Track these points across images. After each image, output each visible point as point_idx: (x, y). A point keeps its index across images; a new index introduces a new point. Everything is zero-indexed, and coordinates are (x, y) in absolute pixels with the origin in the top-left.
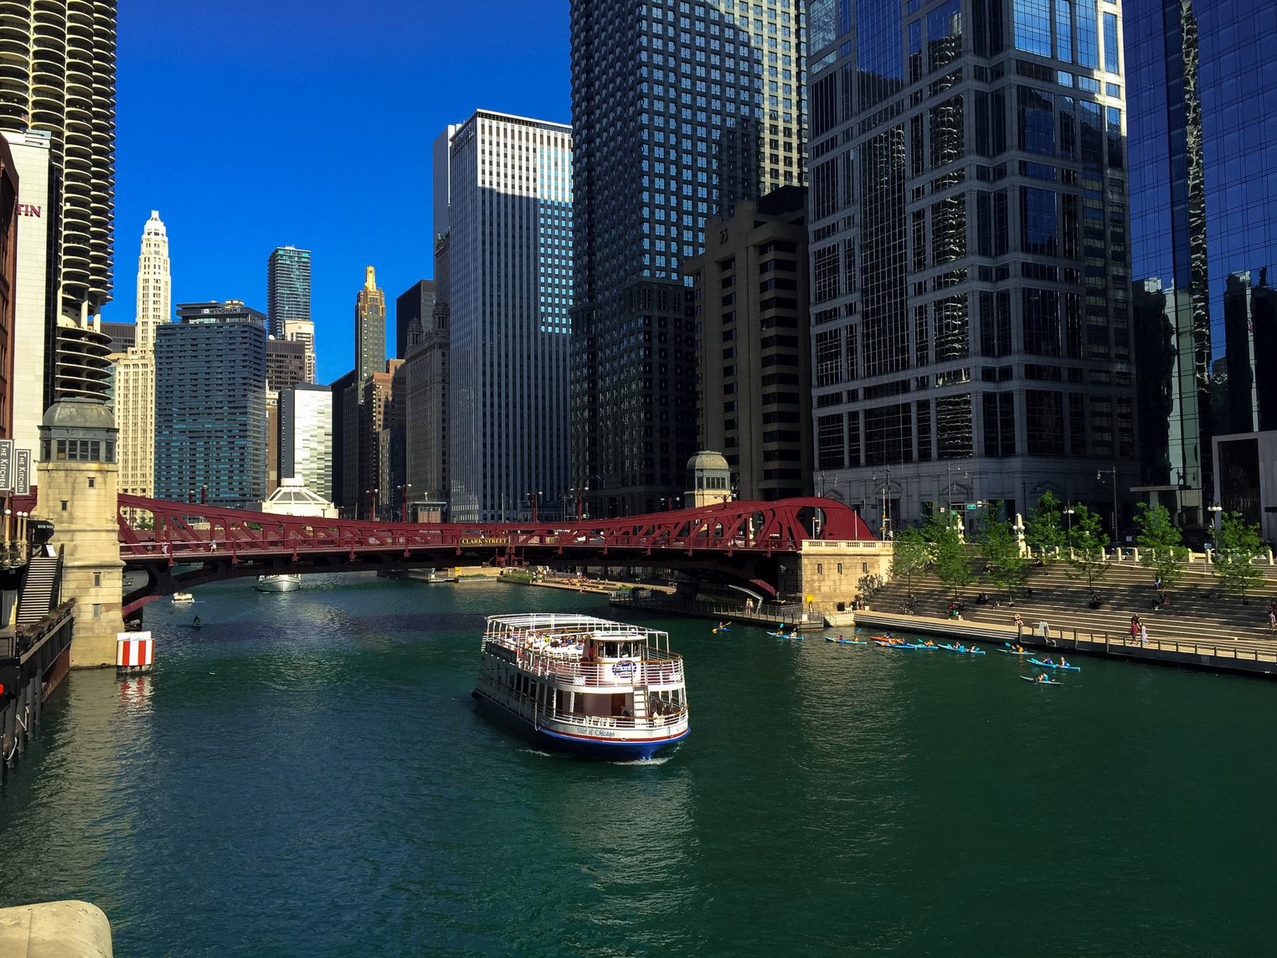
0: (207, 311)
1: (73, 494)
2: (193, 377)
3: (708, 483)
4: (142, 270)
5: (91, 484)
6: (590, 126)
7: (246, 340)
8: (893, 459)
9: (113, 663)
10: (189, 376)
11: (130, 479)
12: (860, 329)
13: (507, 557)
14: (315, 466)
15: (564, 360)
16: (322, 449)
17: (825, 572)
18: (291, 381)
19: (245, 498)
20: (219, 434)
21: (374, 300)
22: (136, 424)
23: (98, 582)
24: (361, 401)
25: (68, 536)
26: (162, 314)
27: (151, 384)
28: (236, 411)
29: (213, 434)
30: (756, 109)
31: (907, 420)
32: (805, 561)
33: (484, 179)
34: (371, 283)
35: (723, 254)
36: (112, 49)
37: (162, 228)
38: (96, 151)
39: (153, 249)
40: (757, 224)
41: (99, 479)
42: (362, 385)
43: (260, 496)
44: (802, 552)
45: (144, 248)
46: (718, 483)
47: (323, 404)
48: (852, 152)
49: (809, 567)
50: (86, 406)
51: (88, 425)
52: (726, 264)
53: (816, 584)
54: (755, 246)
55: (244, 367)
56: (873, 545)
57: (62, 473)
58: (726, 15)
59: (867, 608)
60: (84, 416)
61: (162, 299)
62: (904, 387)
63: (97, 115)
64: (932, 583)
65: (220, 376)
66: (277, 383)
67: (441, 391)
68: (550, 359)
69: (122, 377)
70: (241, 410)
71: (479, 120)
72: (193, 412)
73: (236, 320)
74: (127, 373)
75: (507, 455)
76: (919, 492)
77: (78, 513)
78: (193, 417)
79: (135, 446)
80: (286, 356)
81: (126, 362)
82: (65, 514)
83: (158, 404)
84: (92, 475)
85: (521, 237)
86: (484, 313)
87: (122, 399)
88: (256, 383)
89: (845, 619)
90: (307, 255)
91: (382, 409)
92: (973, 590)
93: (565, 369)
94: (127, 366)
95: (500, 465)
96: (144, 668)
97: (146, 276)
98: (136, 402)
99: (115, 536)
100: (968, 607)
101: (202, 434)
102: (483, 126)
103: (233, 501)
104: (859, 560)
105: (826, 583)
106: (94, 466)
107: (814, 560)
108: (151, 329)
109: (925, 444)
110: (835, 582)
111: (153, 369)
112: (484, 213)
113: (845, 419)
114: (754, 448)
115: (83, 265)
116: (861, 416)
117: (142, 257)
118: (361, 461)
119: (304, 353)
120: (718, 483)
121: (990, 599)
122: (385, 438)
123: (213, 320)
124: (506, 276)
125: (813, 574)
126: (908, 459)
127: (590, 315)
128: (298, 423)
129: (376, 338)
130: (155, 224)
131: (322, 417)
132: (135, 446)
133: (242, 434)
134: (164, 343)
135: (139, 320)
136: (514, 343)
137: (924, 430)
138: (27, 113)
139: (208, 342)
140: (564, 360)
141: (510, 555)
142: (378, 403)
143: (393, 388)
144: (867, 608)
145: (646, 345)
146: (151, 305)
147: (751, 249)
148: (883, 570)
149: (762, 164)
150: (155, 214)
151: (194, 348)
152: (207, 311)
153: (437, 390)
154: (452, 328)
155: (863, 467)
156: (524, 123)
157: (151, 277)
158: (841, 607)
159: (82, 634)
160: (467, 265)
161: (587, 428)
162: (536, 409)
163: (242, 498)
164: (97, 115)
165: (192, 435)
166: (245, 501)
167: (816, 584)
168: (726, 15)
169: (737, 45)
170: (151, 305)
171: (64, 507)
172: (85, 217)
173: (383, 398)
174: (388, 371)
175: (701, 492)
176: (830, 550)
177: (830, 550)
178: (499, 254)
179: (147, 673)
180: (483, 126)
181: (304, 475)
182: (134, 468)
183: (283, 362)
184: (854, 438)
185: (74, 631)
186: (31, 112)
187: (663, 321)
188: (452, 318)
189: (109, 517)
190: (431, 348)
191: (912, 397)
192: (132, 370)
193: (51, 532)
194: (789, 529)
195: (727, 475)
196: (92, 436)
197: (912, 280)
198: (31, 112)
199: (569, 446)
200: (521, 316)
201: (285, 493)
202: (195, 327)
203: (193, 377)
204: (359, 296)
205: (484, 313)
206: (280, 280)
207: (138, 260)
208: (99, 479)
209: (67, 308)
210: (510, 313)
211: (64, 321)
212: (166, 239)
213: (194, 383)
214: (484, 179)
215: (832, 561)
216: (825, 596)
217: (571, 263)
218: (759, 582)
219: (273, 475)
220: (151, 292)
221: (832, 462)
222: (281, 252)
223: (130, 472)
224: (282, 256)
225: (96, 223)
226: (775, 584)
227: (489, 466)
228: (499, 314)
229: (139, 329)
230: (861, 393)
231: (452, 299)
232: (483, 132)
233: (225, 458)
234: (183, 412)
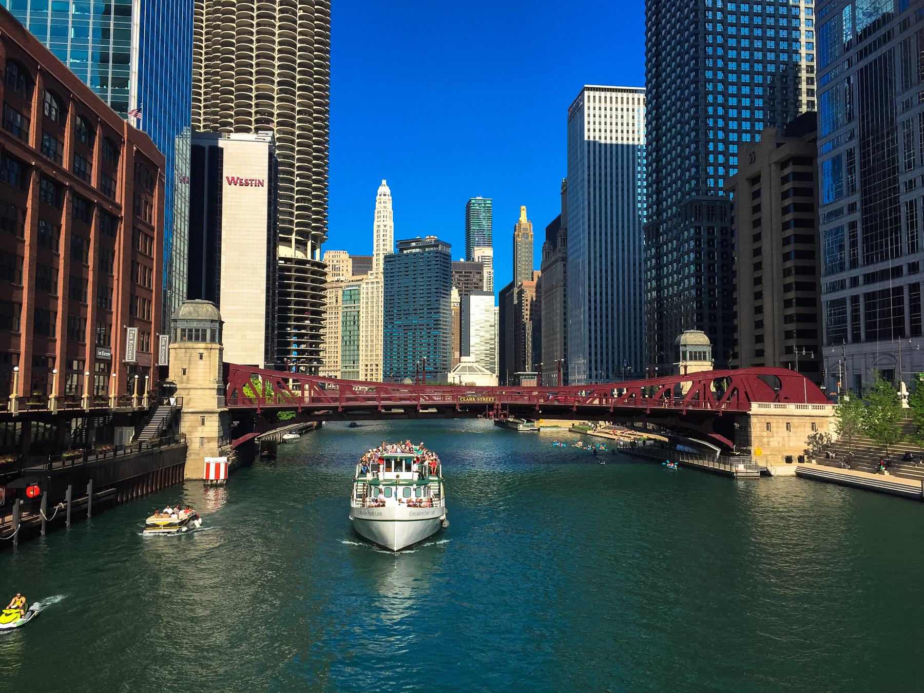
0: (414, 244)
2: (406, 289)
5: (201, 357)
6: (657, 86)
7: (438, 263)
8: (885, 336)
9: (201, 477)
10: (403, 289)
11: (369, 358)
13: (495, 412)
14: (484, 348)
15: (640, 264)
16: (488, 336)
17: (774, 429)
18: (471, 287)
19: (437, 370)
20: (422, 327)
21: (526, 229)
22: (372, 322)
23: (203, 424)
24: (516, 302)
25: (186, 392)
26: (388, 248)
27: (382, 295)
30: (794, 55)
31: (900, 301)
32: (753, 420)
34: (523, 218)
35: (751, 171)
36: (327, 74)
37: (388, 191)
38: (316, 142)
39: (383, 205)
40: (779, 145)
43: (446, 369)
44: (750, 413)
46: (700, 356)
47: (488, 304)
49: (758, 425)
50: (200, 305)
51: (200, 318)
52: (755, 180)
53: (765, 440)
55: (437, 281)
56: (823, 408)
57: (183, 350)
59: (814, 461)
60: (197, 312)
63: (316, 119)
64: (867, 443)
65: (422, 288)
66: (465, 291)
67: (563, 293)
71: (586, 93)
73: (432, 249)
74: (367, 288)
75: (613, 338)
77: (192, 377)
78: (406, 316)
79: (372, 336)
80: (471, 273)
81: (367, 281)
82: (185, 377)
84: (201, 351)
85: (617, 175)
86: (589, 233)
88: (444, 292)
90: (489, 202)
91: (528, 307)
93: (640, 271)
94: (367, 283)
95: (607, 345)
97: (379, 223)
99: (215, 392)
101: (411, 327)
102: (589, 97)
104: (809, 421)
105: (775, 439)
106: (202, 345)
107: (763, 419)
108: (382, 257)
110: (783, 438)
113: (848, 302)
114: (776, 329)
115: (308, 217)
116: (862, 299)
117: (376, 211)
118: (516, 344)
120: (700, 356)
121: (915, 457)
122: (529, 326)
123: (418, 250)
125: (763, 431)
127: (658, 230)
128: (473, 319)
129: (527, 257)
130: (384, 189)
131: (488, 314)
132: (372, 336)
133: (435, 327)
135: (375, 253)
136: (612, 254)
138: (273, 122)
139: (415, 265)
140: (640, 264)
142: (526, 303)
144: (814, 461)
146: (381, 243)
147: (773, 166)
149: (800, 98)
150: (384, 182)
151: (406, 269)
152: (414, 244)
153: (560, 292)
154: (569, 245)
155: (863, 342)
156: (624, 91)
157: (382, 224)
158: (789, 460)
159: (192, 457)
160: (578, 199)
161: (695, 318)
163: (435, 370)
164: (316, 119)
165: (405, 328)
166: (437, 372)
167: (765, 440)
170: (381, 243)
171: (184, 373)
172: (309, 186)
173: (529, 299)
174: (533, 280)
178: (600, 189)
179: (221, 485)
180: (589, 97)
181: (476, 355)
184: (856, 318)
185: (187, 455)
186: (276, 121)
187: (710, 230)
188: (569, 239)
189: (212, 379)
190: (556, 261)
191: (904, 281)
192: (370, 286)
193: (176, 389)
194: (746, 392)
195: (708, 350)
196: (202, 325)
198: (276, 121)
201: (463, 367)
202: (407, 255)
203: (406, 289)
204: (515, 227)
209: (298, 246)
211: (284, 251)
212: (391, 198)
215: (781, 420)
216: (773, 449)
218: (717, 437)
219: (457, 354)
220: (382, 233)
222: (473, 201)
224: (474, 204)
225: (316, 189)
228: (596, 324)
229: (374, 259)
230: (861, 279)
231: (569, 225)
232: (589, 101)
233: (425, 343)
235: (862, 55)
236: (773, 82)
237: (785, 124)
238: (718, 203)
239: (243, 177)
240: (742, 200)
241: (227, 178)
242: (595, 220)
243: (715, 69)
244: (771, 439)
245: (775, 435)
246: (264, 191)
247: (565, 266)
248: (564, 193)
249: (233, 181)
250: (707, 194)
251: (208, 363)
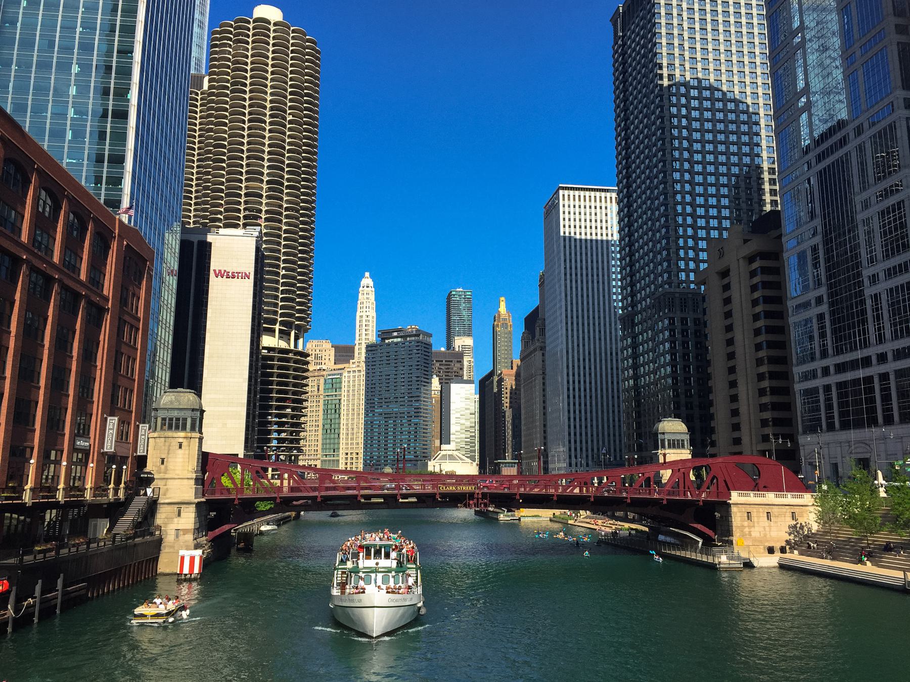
0: (395, 334)
1: (168, 454)
3: (669, 444)
4: (359, 310)
5: (180, 447)
7: (419, 352)
8: (859, 425)
11: (349, 446)
12: (827, 316)
14: (464, 436)
15: (617, 354)
17: (755, 519)
19: (417, 459)
23: (179, 515)
24: (495, 390)
25: (163, 482)
26: (370, 337)
27: (363, 383)
28: (413, 399)
29: (399, 415)
30: (756, 158)
31: (871, 390)
32: (734, 509)
33: (565, 230)
34: (503, 309)
35: (721, 266)
38: (302, 237)
39: (365, 296)
40: (746, 241)
41: (185, 443)
42: (496, 379)
43: (427, 457)
44: (731, 502)
45: (360, 296)
46: (678, 444)
47: (468, 392)
48: (812, 179)
49: (739, 514)
50: (182, 394)
51: (181, 407)
52: (725, 274)
53: (747, 530)
54: (744, 258)
55: (418, 369)
56: (801, 497)
57: (163, 439)
58: (728, 93)
60: (179, 401)
61: (370, 328)
62: (866, 362)
63: (303, 215)
64: (847, 533)
65: (403, 376)
66: (446, 379)
68: (611, 354)
69: (346, 380)
70: (416, 399)
71: (561, 192)
72: (386, 401)
73: (413, 338)
76: (886, 451)
78: (387, 404)
80: (451, 361)
81: (349, 370)
82: (163, 467)
83: (366, 396)
84: (181, 440)
86: (567, 323)
87: (346, 394)
89: (773, 560)
91: (508, 395)
92: (883, 537)
94: (349, 372)
96: (193, 576)
97: (362, 314)
98: (354, 395)
99: (193, 482)
100: (872, 555)
101: (392, 415)
103: (411, 461)
104: (788, 511)
105: (757, 529)
106: (182, 434)
108: (364, 346)
109: (888, 411)
111: (364, 373)
112: (565, 255)
113: (821, 391)
114: (752, 418)
117: (359, 302)
119: (463, 358)
120: (678, 444)
122: (509, 414)
123: (399, 340)
124: (582, 296)
126: (873, 422)
127: (633, 320)
130: (367, 281)
131: (468, 402)
132: (353, 424)
133: (416, 414)
134: (371, 356)
135: (357, 342)
137: (886, 398)
138: (261, 218)
140: (617, 354)
141: (478, 499)
142: (506, 391)
143: (516, 379)
145: (671, 327)
146: (364, 332)
147: (741, 261)
148: (811, 520)
149: (764, 198)
150: (367, 274)
152: (395, 334)
153: (539, 380)
154: (547, 335)
155: (838, 431)
157: (364, 314)
158: (771, 550)
159: (167, 550)
161: (672, 406)
162: (613, 391)
163: (415, 458)
164: (303, 215)
165: (386, 416)
166: (417, 461)
167: (747, 530)
168: (728, 93)
169: (738, 114)
170: (364, 332)
171: (163, 463)
173: (509, 387)
175: (663, 452)
176: (759, 500)
177: (759, 500)
179: (195, 579)
180: (564, 195)
181: (456, 443)
182: (352, 439)
183: (449, 365)
184: (829, 407)
186: (263, 217)
187: (684, 321)
188: (547, 329)
189: (190, 469)
192: (352, 374)
193: (153, 479)
195: (687, 437)
197: (866, 273)
199: (622, 419)
200: (594, 324)
202: (389, 344)
204: (495, 318)
205: (567, 323)
206: (453, 311)
207: (357, 304)
208: (185, 443)
209: (282, 335)
210: (591, 322)
212: (373, 289)
213: (388, 381)
214: (565, 230)
216: (755, 540)
217: (619, 283)
218: (699, 527)
219: (437, 442)
221: (813, 428)
223: (350, 442)
224: (454, 295)
226: (713, 527)
227: (572, 434)
228: (587, 275)
229: (357, 348)
230: (832, 369)
234: (381, 401)
235: (820, 158)
236: (737, 183)
237: (751, 221)
238: (690, 296)
239: (230, 269)
240: (712, 292)
241: (215, 271)
242: (572, 311)
243: (682, 171)
244: (752, 529)
245: (756, 525)
246: (249, 284)
247: (543, 355)
248: (541, 285)
249: (220, 274)
250: (679, 287)
251: (187, 452)
